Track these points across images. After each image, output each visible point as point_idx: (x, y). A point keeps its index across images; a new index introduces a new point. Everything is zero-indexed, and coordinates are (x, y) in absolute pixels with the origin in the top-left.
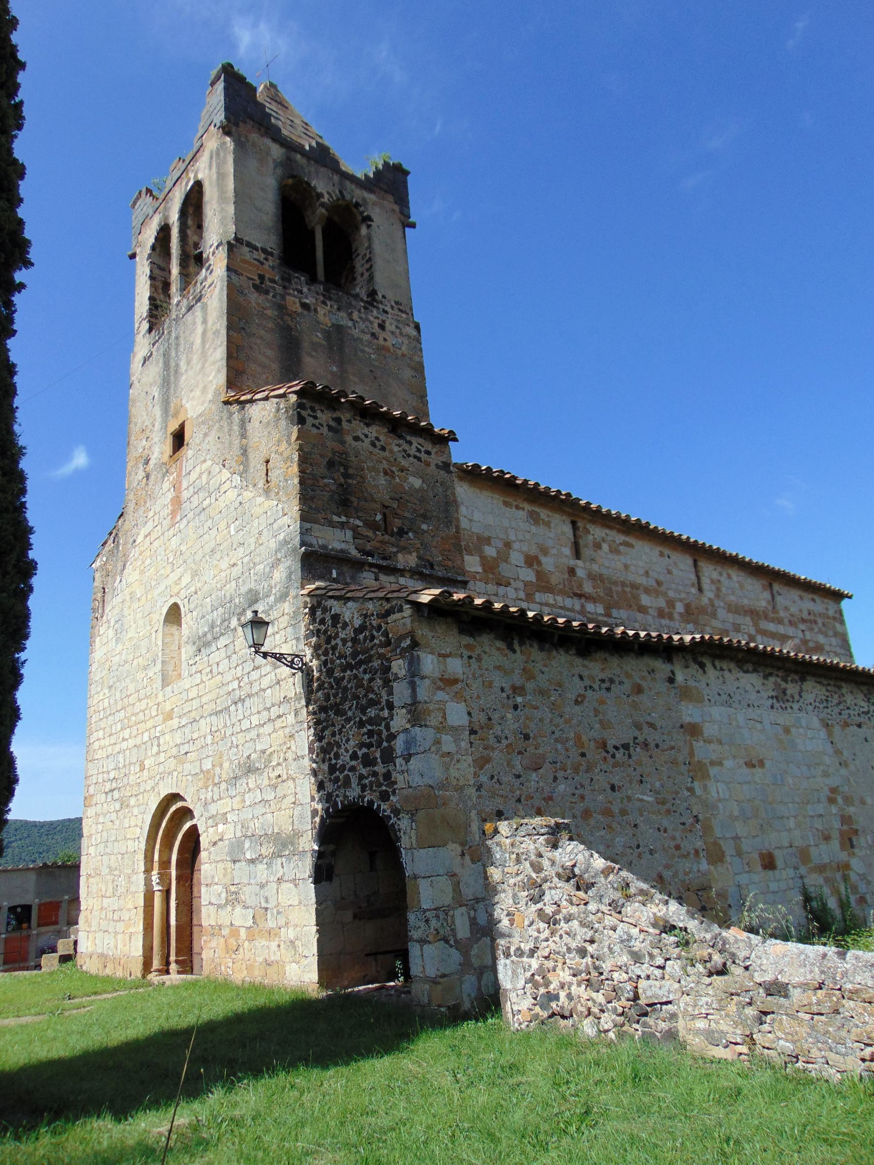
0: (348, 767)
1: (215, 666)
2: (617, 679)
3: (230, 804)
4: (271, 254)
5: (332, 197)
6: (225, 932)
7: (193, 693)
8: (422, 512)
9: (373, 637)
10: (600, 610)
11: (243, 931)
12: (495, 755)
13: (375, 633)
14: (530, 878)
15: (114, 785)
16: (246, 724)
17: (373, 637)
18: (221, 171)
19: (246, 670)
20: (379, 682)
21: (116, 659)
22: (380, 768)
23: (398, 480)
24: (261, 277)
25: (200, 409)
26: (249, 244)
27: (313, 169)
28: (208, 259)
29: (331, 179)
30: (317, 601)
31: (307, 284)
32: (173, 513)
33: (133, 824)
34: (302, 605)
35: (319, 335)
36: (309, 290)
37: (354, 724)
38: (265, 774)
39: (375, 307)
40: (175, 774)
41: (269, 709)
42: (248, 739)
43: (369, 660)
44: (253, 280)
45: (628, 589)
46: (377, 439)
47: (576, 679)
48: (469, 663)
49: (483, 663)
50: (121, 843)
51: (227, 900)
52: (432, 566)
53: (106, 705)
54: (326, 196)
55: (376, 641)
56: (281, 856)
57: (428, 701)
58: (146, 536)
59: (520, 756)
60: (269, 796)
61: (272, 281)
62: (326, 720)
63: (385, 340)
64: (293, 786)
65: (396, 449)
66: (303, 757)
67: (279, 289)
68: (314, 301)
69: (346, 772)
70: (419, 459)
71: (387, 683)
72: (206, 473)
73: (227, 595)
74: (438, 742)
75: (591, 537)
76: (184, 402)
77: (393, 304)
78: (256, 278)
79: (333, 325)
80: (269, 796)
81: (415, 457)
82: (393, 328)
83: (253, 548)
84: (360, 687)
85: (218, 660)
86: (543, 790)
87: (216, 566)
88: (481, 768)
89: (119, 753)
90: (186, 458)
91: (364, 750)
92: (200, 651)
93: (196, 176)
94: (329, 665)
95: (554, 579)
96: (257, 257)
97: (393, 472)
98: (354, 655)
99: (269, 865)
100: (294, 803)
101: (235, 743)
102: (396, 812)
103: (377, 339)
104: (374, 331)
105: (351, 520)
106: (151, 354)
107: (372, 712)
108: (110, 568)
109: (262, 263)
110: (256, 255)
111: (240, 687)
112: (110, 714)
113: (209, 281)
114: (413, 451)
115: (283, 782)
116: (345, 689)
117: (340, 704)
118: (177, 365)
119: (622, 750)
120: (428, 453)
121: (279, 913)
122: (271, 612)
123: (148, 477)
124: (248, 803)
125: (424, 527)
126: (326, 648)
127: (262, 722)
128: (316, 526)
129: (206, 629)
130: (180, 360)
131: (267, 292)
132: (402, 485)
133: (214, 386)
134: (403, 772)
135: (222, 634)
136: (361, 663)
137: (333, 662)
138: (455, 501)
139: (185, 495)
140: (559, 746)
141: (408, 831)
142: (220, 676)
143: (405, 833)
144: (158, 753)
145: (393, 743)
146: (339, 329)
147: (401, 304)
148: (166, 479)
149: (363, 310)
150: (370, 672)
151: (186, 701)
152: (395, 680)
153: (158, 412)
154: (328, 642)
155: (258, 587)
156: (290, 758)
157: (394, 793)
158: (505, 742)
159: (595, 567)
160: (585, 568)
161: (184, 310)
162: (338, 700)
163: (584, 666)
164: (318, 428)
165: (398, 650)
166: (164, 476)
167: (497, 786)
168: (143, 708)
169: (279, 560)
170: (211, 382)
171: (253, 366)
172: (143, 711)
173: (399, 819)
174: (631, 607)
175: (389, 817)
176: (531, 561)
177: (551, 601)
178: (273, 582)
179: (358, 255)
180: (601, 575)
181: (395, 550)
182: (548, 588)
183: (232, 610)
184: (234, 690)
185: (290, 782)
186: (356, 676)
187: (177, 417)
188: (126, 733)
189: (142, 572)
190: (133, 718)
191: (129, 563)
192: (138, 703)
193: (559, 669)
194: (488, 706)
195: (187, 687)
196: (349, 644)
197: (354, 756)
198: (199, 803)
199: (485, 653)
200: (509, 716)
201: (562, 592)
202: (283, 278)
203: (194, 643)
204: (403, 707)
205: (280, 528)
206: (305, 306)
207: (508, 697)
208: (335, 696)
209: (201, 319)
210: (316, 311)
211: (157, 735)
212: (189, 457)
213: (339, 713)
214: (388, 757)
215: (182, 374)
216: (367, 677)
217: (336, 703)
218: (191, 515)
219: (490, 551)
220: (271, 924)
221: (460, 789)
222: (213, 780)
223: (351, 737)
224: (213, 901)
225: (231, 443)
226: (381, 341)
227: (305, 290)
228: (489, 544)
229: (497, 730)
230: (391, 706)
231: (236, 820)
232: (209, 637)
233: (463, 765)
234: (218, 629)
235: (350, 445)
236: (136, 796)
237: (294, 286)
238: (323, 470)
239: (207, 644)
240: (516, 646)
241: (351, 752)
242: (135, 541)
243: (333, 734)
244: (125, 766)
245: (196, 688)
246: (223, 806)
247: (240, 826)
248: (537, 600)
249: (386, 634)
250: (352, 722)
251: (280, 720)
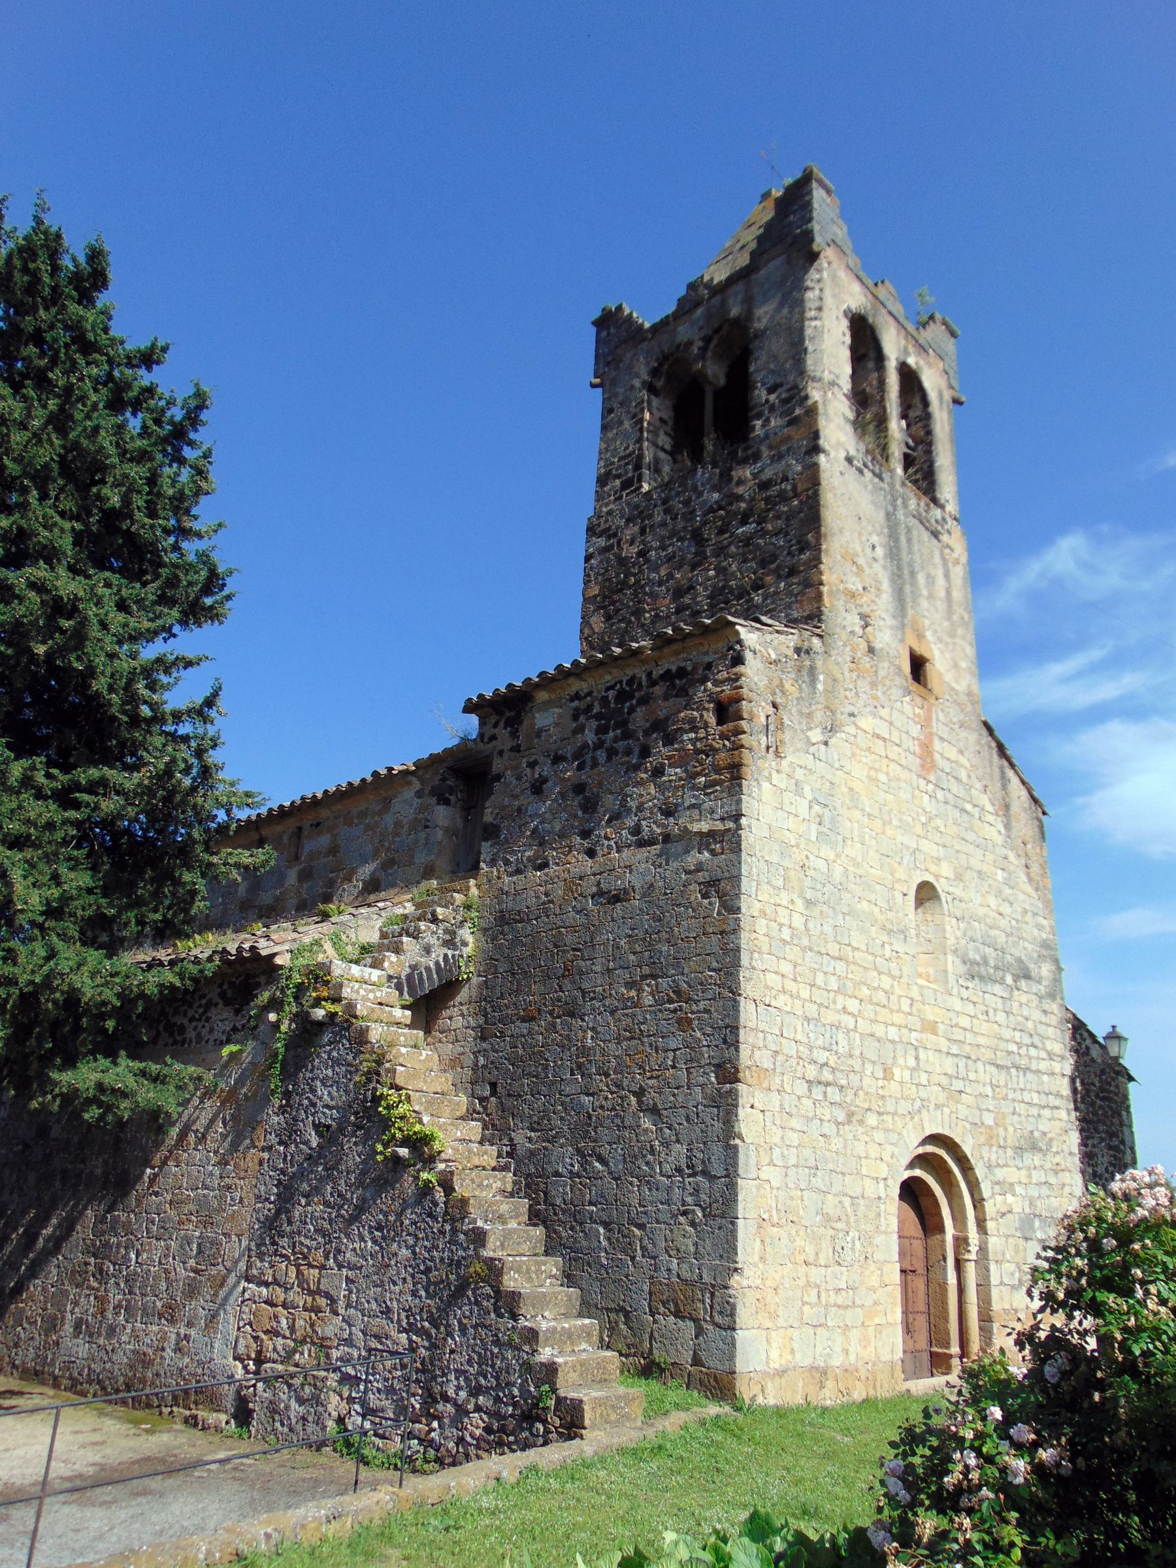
124: (1034, 1181)
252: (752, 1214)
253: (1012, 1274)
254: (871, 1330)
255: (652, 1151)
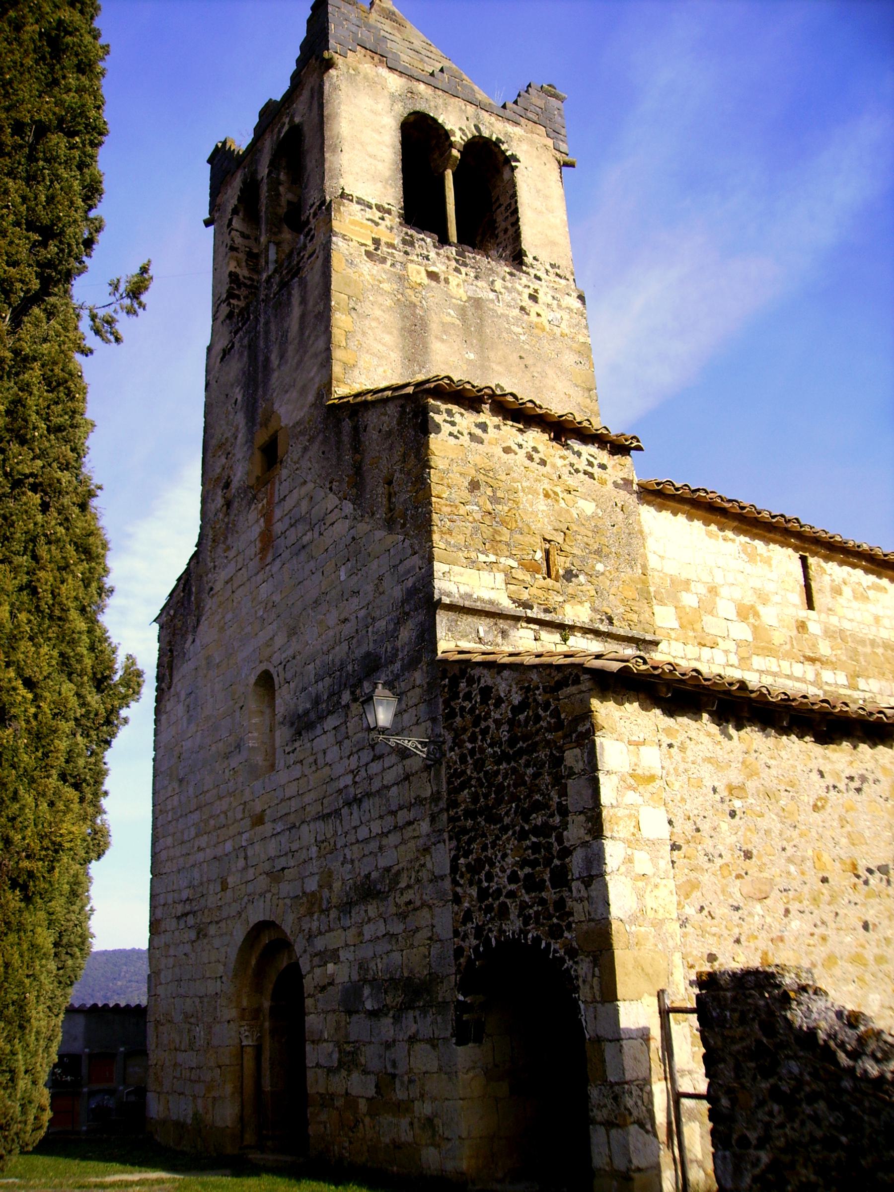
0: (504, 892)
1: (320, 756)
2: (871, 777)
3: (343, 938)
4: (389, 212)
5: (465, 134)
6: (339, 1103)
7: (291, 790)
8: (596, 547)
9: (538, 718)
10: (842, 679)
11: (363, 1106)
12: (705, 878)
13: (541, 712)
14: (759, 1042)
15: (188, 908)
16: (363, 833)
17: (538, 718)
18: (370, 406)
19: (364, 761)
20: (547, 779)
21: (188, 744)
22: (550, 895)
23: (562, 504)
24: (376, 242)
25: (298, 415)
26: (360, 201)
27: (440, 101)
28: (308, 222)
29: (465, 111)
30: (461, 669)
31: (435, 247)
32: (264, 550)
33: (213, 959)
34: (439, 675)
35: (452, 312)
36: (438, 254)
37: (514, 834)
38: (391, 899)
39: (525, 272)
40: (268, 895)
41: (393, 813)
42: (367, 852)
43: (534, 748)
44: (365, 245)
45: (880, 651)
46: (535, 449)
47: (815, 776)
48: (669, 753)
49: (689, 752)
50: (198, 982)
51: (340, 1061)
52: (610, 620)
53: (176, 803)
54: (458, 134)
55: (543, 724)
56: (413, 1008)
57: (615, 803)
58: (227, 583)
59: (738, 882)
60: (397, 928)
61: (391, 245)
62: (473, 829)
63: (538, 315)
64: (428, 916)
65: (560, 463)
66: (442, 878)
67: (399, 256)
68: (444, 268)
69: (502, 899)
70: (591, 476)
71: (559, 781)
72: (307, 499)
73: (337, 660)
74: (630, 860)
75: (826, 578)
76: (276, 406)
77: (549, 268)
78: (369, 242)
79: (470, 298)
80: (397, 928)
81: (585, 473)
82: (549, 300)
83: (371, 598)
84: (520, 786)
85: (325, 747)
86: (770, 927)
87: (321, 622)
88: (687, 896)
89: (193, 866)
90: (280, 479)
91: (527, 870)
92: (300, 734)
93: (291, 121)
94: (478, 756)
95: (778, 638)
96: (371, 217)
97: (556, 493)
98: (512, 742)
99: (397, 1020)
100: (430, 939)
101: (348, 857)
102: (572, 953)
103: (528, 314)
104: (523, 304)
105: (502, 560)
106: (233, 346)
107: (538, 819)
108: (179, 624)
109: (377, 224)
110: (369, 214)
111: (355, 783)
112: (181, 816)
113: (310, 249)
114: (582, 465)
115: (415, 909)
116: (500, 788)
117: (493, 807)
118: (267, 360)
119: (878, 875)
120: (603, 467)
121: (411, 1081)
122: (396, 684)
123: (228, 504)
124: (367, 937)
125: (600, 567)
126: (474, 733)
127: (385, 830)
128: (456, 569)
129: (308, 706)
130: (270, 352)
131: (383, 260)
132: (568, 511)
133: (316, 386)
134: (581, 900)
135: (330, 713)
136: (520, 753)
137: (482, 750)
138: (641, 532)
139: (278, 528)
140: (792, 868)
141: (589, 979)
142: (328, 768)
143: (584, 981)
144: (245, 869)
145: (567, 860)
146: (477, 303)
147: (559, 267)
148: (253, 506)
149: (508, 277)
150: (535, 765)
151: (282, 801)
152: (569, 776)
153: (240, 419)
154: (476, 723)
155: (378, 650)
156: (425, 879)
157: (569, 928)
158: (719, 862)
159: (834, 620)
160: (819, 622)
161: (275, 287)
162: (490, 803)
163: (825, 758)
164: (457, 437)
165: (574, 735)
166: (250, 504)
167: (708, 920)
168: (224, 808)
169: (407, 614)
170: (312, 379)
171: (367, 357)
172: (225, 813)
173: (576, 963)
174: (884, 674)
175: (562, 960)
176: (745, 613)
177: (775, 669)
178: (399, 644)
179: (500, 205)
180: (842, 631)
181: (561, 599)
182: (769, 650)
183: (343, 680)
184: (346, 787)
185: (425, 910)
186: (514, 770)
187: (266, 426)
188: (203, 841)
189: (222, 629)
190: (212, 822)
191: (204, 618)
192: (218, 802)
193: (791, 762)
194: (696, 812)
195: (282, 782)
196: (506, 727)
197: (513, 878)
198: (301, 936)
199: (690, 739)
200: (724, 827)
201: (787, 656)
202: (404, 242)
203: (292, 724)
204: (581, 813)
205: (409, 572)
206: (433, 276)
207: (722, 801)
208: (486, 796)
209: (299, 299)
210: (447, 281)
211: (244, 844)
212: (284, 478)
213: (493, 819)
214: (561, 878)
215: (273, 370)
216: (530, 771)
217: (487, 805)
218: (286, 555)
219: (689, 600)
220: (401, 1094)
221: (658, 924)
222: (320, 905)
223: (509, 851)
224: (322, 1062)
225: (339, 458)
226: (533, 317)
227: (432, 255)
228: (687, 590)
229: (708, 845)
230: (563, 811)
231: (351, 958)
232: (313, 716)
233: (662, 892)
234: (324, 706)
235: (499, 458)
236: (217, 923)
237: (419, 251)
238: (465, 494)
239: (310, 726)
240: (732, 731)
241: (508, 872)
242: (211, 589)
243: (485, 848)
244: (202, 884)
245: (297, 782)
246: (333, 940)
247: (357, 967)
248: (755, 667)
249: (556, 713)
250: (510, 833)
251: (411, 828)
252: (152, 1019)
253: (330, 1055)
254: (210, 1100)
255: (128, 987)
